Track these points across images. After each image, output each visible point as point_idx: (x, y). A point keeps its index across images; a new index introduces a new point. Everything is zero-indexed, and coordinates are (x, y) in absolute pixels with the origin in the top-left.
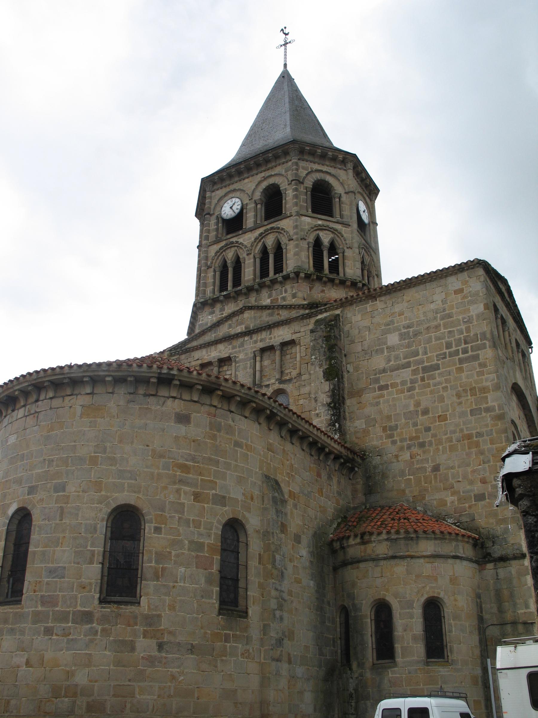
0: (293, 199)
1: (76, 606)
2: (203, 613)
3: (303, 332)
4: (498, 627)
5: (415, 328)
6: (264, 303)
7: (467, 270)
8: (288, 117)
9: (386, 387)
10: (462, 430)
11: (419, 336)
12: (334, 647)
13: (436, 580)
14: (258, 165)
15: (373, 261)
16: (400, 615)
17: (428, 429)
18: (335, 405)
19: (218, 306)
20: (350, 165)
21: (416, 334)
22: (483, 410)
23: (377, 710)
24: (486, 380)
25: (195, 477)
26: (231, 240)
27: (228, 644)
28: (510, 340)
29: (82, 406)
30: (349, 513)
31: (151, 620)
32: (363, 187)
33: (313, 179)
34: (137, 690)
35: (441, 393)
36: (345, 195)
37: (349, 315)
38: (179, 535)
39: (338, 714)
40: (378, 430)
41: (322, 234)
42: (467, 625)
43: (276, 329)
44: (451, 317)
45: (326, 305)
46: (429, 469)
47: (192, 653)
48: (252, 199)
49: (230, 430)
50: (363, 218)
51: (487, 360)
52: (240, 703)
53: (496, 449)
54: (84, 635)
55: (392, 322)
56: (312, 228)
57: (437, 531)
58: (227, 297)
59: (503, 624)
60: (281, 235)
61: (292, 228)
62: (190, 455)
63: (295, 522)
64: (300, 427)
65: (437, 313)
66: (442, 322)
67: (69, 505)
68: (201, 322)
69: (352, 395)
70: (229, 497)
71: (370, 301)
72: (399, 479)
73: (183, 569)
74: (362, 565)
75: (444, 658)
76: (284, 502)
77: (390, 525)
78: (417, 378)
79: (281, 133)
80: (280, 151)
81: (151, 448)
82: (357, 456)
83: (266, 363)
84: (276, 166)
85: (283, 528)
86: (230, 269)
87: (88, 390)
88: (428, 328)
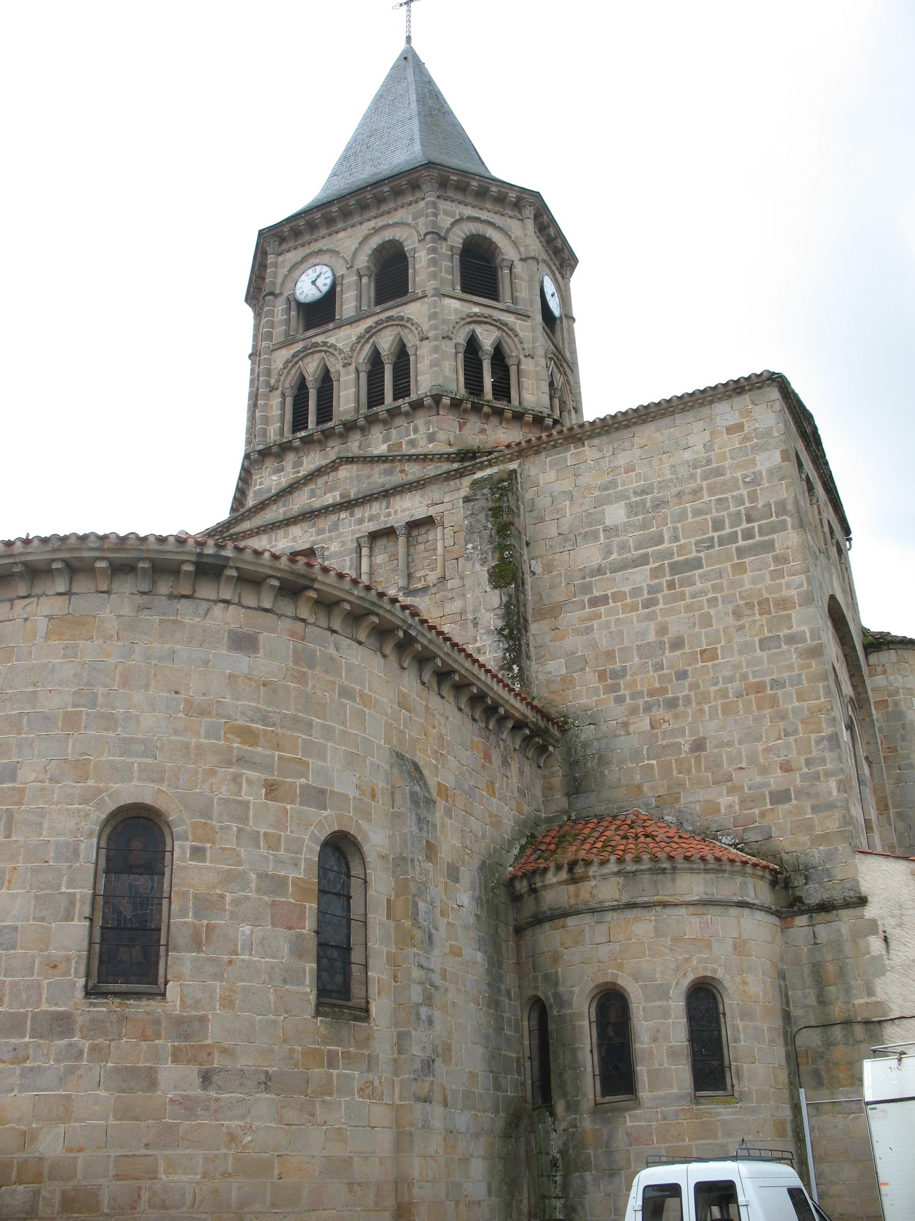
0: (430, 268)
1: (38, 1003)
2: (287, 1012)
3: (450, 503)
4: (819, 1030)
5: (655, 494)
6: (376, 452)
7: (750, 390)
8: (415, 124)
9: (604, 600)
10: (744, 677)
11: (663, 508)
12: (519, 1074)
13: (709, 946)
14: (363, 207)
15: (569, 384)
16: (644, 1012)
17: (682, 675)
18: (511, 632)
19: (291, 458)
20: (529, 212)
21: (658, 505)
22: (783, 639)
23: (634, 1189)
24: (788, 586)
25: (268, 752)
26: (314, 340)
27: (335, 1072)
28: (821, 520)
29: (50, 618)
30: (539, 828)
31: (187, 1028)
32: (551, 253)
33: (465, 234)
34: (162, 1165)
35: (706, 609)
36: (520, 263)
37: (533, 471)
38: (239, 863)
39: (529, 1198)
40: (590, 677)
41: (479, 330)
42: (765, 1028)
43: (398, 497)
44: (722, 475)
45: (490, 453)
46: (686, 748)
47: (267, 1090)
48: (351, 267)
49: (331, 665)
50: (551, 306)
51: (790, 551)
52: (359, 1184)
53: (809, 709)
54: (54, 1060)
55: (613, 484)
56: (463, 319)
57: (710, 857)
58: (308, 442)
59: (827, 1026)
60: (406, 331)
61: (426, 319)
62: (259, 710)
63: (449, 844)
64: (456, 666)
65: (695, 467)
66: (704, 484)
67: (23, 807)
68: (258, 487)
69: (541, 614)
70: (332, 792)
71: (572, 445)
72: (630, 765)
73: (247, 929)
74: (571, 922)
75: (725, 1090)
76: (430, 802)
77: (622, 847)
78: (661, 584)
79: (404, 151)
80: (404, 182)
81: (184, 696)
82: (553, 723)
83: (380, 559)
84: (396, 210)
85: (431, 850)
86: (310, 391)
87: (61, 587)
88: (679, 494)
